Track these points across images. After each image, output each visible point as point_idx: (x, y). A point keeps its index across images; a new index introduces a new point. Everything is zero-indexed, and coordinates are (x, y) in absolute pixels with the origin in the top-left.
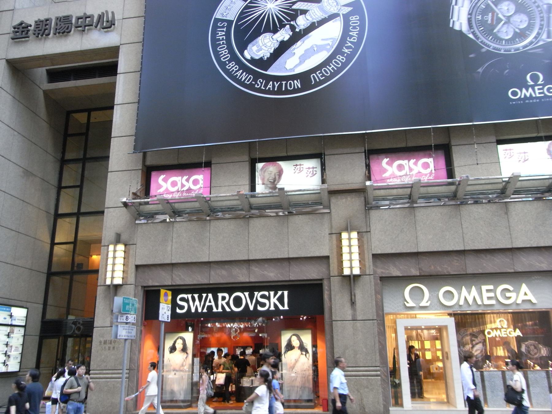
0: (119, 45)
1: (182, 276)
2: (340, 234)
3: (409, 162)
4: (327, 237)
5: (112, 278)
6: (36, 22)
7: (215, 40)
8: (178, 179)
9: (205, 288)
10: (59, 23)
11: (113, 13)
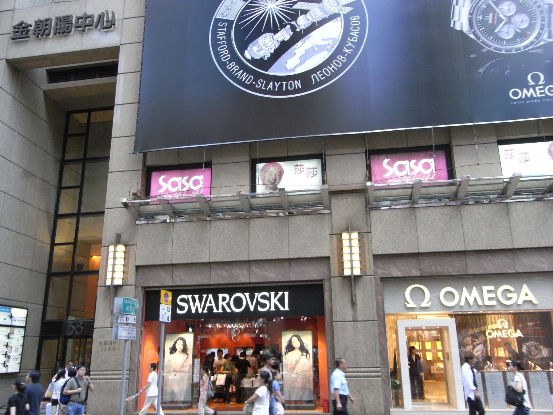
0: (119, 45)
1: (182, 277)
2: (341, 234)
3: (409, 162)
4: (328, 237)
5: (113, 278)
6: (36, 22)
7: (215, 40)
8: (178, 179)
9: (205, 289)
10: (59, 23)
11: (113, 13)
